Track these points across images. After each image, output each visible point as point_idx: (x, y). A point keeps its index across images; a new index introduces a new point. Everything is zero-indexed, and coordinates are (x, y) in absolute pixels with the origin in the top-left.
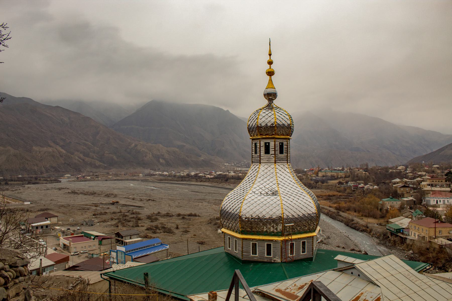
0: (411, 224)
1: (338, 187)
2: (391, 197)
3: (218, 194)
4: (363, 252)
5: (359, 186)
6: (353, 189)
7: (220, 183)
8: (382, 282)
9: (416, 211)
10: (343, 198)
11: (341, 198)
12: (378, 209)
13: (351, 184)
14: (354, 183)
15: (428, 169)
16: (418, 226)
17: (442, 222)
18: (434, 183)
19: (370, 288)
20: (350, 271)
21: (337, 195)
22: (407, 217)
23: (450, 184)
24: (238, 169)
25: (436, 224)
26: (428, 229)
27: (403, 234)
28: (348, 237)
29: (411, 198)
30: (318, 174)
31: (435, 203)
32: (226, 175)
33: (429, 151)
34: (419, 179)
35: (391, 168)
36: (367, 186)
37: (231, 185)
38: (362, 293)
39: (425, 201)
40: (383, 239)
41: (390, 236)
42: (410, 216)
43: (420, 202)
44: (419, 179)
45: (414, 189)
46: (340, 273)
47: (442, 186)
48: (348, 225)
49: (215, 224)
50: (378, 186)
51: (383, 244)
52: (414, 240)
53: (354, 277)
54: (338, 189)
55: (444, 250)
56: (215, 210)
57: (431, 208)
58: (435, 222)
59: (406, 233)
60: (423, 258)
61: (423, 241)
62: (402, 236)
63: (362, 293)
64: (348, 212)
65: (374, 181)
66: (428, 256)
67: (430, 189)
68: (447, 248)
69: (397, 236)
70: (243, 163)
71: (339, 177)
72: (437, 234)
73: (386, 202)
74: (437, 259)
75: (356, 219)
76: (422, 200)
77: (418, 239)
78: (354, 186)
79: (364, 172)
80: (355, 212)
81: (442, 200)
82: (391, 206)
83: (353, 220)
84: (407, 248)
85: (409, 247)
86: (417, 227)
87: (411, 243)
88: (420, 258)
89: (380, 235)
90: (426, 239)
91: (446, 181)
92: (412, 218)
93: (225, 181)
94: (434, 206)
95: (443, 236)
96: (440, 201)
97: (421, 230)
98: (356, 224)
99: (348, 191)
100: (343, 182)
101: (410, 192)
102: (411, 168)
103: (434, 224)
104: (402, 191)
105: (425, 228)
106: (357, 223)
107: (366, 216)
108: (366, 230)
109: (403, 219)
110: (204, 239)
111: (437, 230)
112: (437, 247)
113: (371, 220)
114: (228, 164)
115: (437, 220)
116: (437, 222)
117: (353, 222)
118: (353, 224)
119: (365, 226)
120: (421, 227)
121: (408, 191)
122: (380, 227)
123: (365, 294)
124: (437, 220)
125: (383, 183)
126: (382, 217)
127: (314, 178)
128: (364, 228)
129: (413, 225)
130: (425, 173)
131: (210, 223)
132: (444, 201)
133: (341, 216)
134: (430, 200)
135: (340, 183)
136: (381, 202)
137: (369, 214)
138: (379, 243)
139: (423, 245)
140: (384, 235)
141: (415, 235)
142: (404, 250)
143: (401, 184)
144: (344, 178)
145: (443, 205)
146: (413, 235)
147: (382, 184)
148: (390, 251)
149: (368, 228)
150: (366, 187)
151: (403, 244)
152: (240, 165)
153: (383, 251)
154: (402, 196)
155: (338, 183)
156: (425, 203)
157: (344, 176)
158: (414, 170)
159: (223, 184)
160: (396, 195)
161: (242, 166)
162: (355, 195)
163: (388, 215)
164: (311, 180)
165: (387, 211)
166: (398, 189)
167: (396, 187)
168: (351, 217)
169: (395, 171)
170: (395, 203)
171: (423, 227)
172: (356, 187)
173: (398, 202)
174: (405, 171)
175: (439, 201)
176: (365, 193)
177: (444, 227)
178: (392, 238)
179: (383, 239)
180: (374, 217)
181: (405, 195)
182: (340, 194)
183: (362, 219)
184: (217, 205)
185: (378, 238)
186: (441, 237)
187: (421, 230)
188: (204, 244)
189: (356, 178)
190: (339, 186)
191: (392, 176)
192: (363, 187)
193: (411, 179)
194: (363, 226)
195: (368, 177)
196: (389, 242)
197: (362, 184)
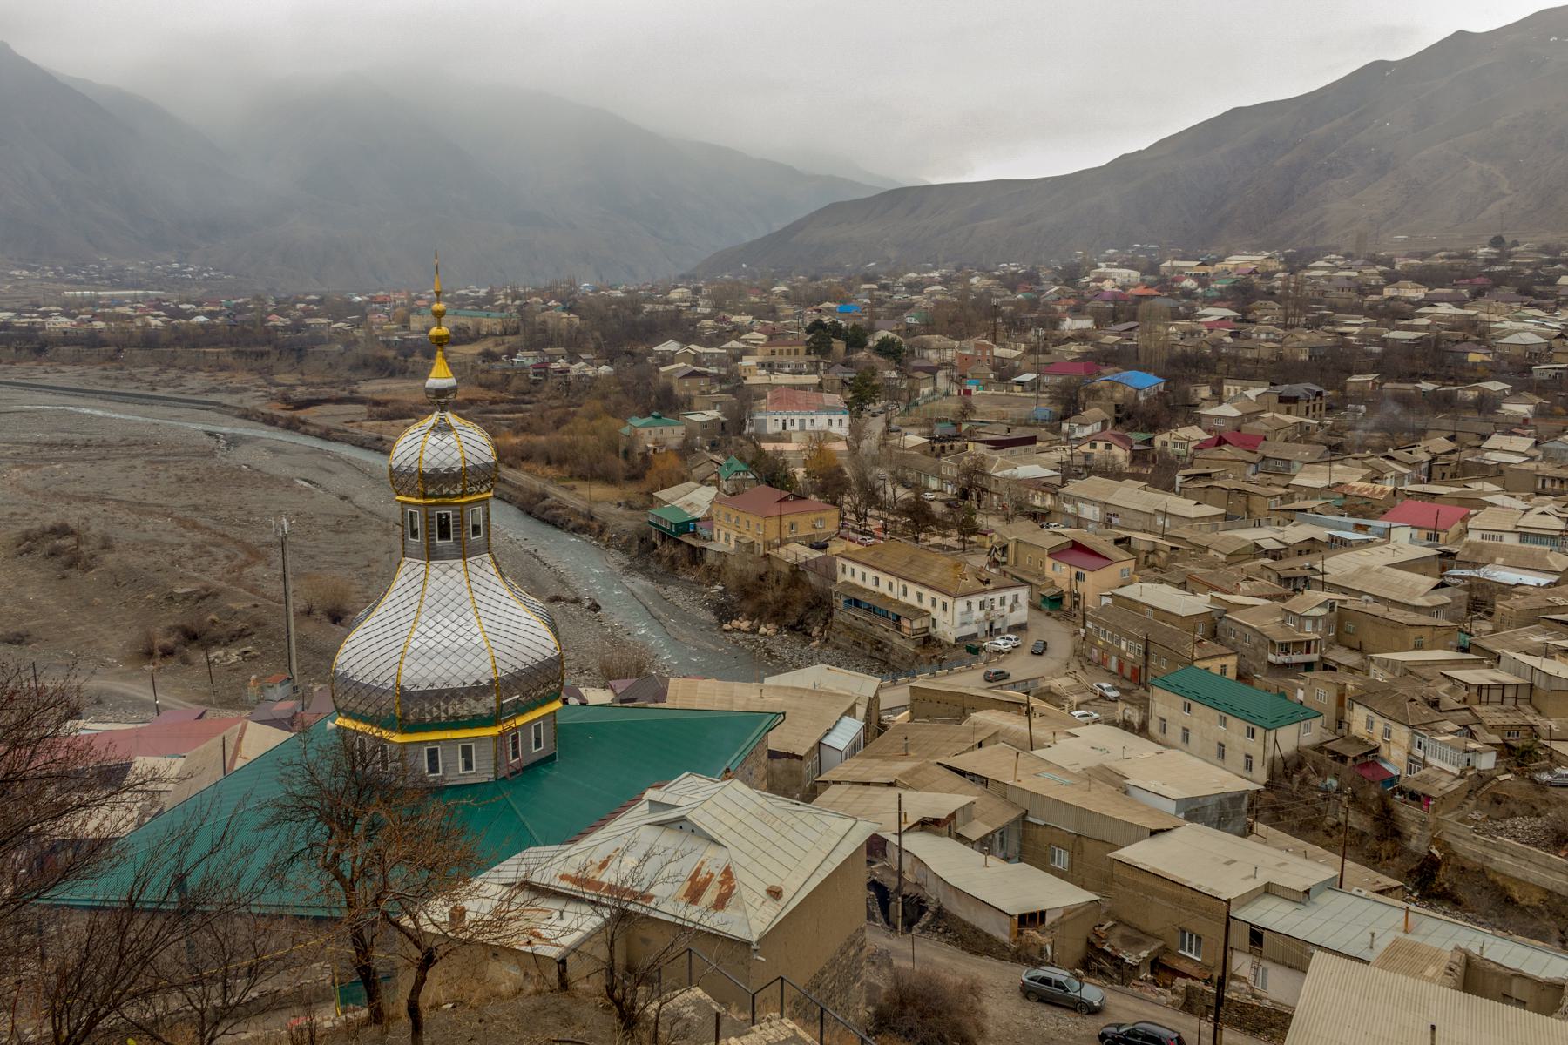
0: (717, 507)
1: (482, 371)
2: (655, 414)
3: (17, 417)
4: (587, 604)
5: (554, 366)
6: (532, 377)
7: (13, 363)
8: (728, 838)
9: (730, 461)
10: (504, 412)
11: (496, 412)
12: (617, 452)
13: (525, 359)
14: (535, 357)
15: (757, 300)
16: (737, 514)
17: (800, 497)
18: (776, 359)
19: (711, 852)
20: (678, 825)
21: (483, 400)
22: (703, 482)
23: (817, 362)
24: (78, 293)
25: (784, 505)
26: (761, 522)
27: (695, 535)
28: (535, 557)
29: (713, 414)
30: (408, 321)
31: (780, 428)
32: (31, 328)
33: (762, 232)
34: (734, 344)
35: (649, 299)
36: (576, 366)
37: (64, 369)
38: (703, 863)
39: (751, 425)
40: (640, 555)
41: (659, 543)
42: (714, 477)
43: (739, 430)
44: (734, 344)
45: (720, 379)
46: (661, 828)
47: (796, 372)
48: (529, 513)
49: (53, 554)
50: (611, 363)
51: (640, 570)
52: (725, 555)
53: (684, 835)
54: (483, 377)
55: (803, 578)
56: (31, 493)
57: (768, 447)
58: (781, 500)
59: (705, 533)
60: (749, 606)
61: (749, 557)
62: (693, 542)
63: (703, 863)
64: (525, 466)
65: (598, 347)
66: (763, 599)
67: (764, 380)
68: (809, 573)
69: (680, 542)
70: (94, 269)
71: (484, 331)
72: (786, 535)
73: (641, 430)
74: (785, 606)
75: (556, 492)
76: (743, 423)
77: (737, 549)
78: (535, 367)
79: (565, 315)
80: (549, 463)
81: (797, 419)
82: (656, 442)
83: (544, 496)
84: (709, 576)
85: (714, 574)
86: (734, 514)
87: (717, 563)
88: (743, 604)
89: (630, 540)
90: (756, 550)
91: (808, 353)
92: (716, 483)
93: (34, 355)
94: (778, 438)
95: (800, 538)
96: (792, 424)
97: (743, 525)
98: (557, 508)
99: (516, 383)
100: (497, 350)
101: (709, 393)
102: (708, 297)
103: (778, 505)
104: (687, 389)
105: (754, 520)
106: (560, 505)
107: (583, 478)
108: (586, 526)
109: (693, 490)
110: (21, 620)
111: (786, 521)
112: (786, 570)
113: (597, 491)
114: (25, 273)
115: (785, 494)
116: (786, 499)
117: (547, 503)
118: (546, 509)
119: (584, 516)
120: (744, 517)
121: (703, 389)
122: (629, 513)
123: (707, 863)
124: (785, 494)
125: (628, 353)
126: (635, 477)
127: (396, 339)
128: (581, 521)
129: (723, 510)
130: (750, 318)
131: (29, 551)
132: (802, 421)
133: (504, 481)
134: (764, 422)
135: (488, 356)
136: (626, 430)
137: (592, 469)
138: (628, 568)
139: (751, 567)
140: (642, 540)
141: (727, 540)
142: (699, 583)
143: (683, 364)
144: (501, 335)
145: (800, 435)
146: (723, 541)
147: (625, 358)
148: (661, 590)
149: (592, 518)
150: (575, 368)
151: (697, 564)
152: (81, 278)
153: (640, 592)
154: (688, 404)
155: (480, 354)
156: (752, 429)
157: (498, 329)
158: (718, 306)
159: (25, 365)
160: (667, 404)
161: (93, 279)
162: (541, 396)
163: (651, 476)
164: (387, 344)
165: (645, 456)
166: (675, 383)
167: (669, 375)
168: (537, 484)
169: (660, 308)
170: (667, 431)
171: (748, 517)
172: (542, 369)
173: (675, 428)
174: (692, 306)
175: (788, 422)
176: (574, 389)
177: (802, 513)
178: (666, 550)
179: (640, 555)
180: (608, 479)
181: (697, 403)
182: (491, 394)
183: (573, 488)
184: (30, 467)
185: (624, 550)
186: (795, 540)
187: (743, 525)
188: (27, 640)
189: (539, 337)
190: (486, 366)
191: (654, 330)
192: (565, 371)
193: (710, 343)
194: (578, 513)
195: (579, 331)
196: (658, 563)
197: (561, 360)
